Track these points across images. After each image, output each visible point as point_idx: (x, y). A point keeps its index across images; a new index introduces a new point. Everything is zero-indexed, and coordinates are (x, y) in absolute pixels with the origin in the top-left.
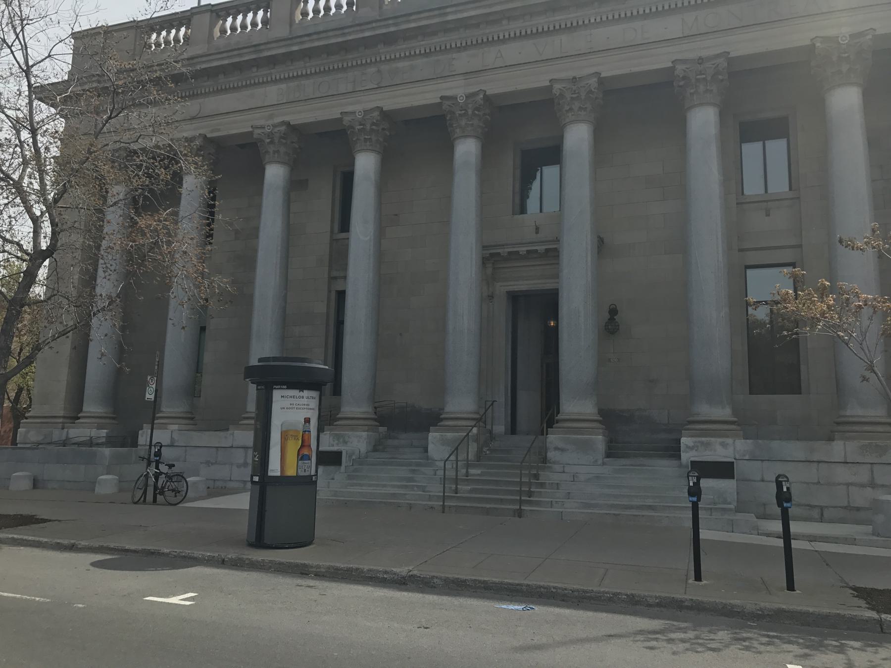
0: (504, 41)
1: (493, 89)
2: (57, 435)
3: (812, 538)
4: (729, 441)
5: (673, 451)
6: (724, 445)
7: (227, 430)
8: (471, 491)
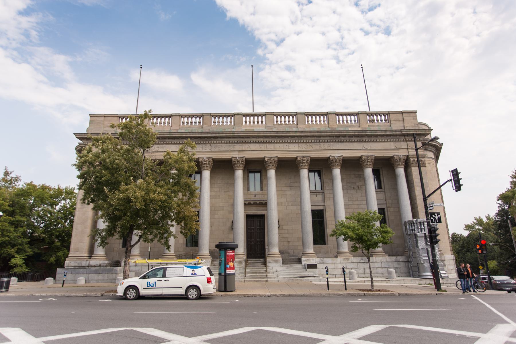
2: (84, 263)
3: (340, 282)
4: (314, 258)
5: (299, 261)
6: (313, 260)
8: (251, 276)
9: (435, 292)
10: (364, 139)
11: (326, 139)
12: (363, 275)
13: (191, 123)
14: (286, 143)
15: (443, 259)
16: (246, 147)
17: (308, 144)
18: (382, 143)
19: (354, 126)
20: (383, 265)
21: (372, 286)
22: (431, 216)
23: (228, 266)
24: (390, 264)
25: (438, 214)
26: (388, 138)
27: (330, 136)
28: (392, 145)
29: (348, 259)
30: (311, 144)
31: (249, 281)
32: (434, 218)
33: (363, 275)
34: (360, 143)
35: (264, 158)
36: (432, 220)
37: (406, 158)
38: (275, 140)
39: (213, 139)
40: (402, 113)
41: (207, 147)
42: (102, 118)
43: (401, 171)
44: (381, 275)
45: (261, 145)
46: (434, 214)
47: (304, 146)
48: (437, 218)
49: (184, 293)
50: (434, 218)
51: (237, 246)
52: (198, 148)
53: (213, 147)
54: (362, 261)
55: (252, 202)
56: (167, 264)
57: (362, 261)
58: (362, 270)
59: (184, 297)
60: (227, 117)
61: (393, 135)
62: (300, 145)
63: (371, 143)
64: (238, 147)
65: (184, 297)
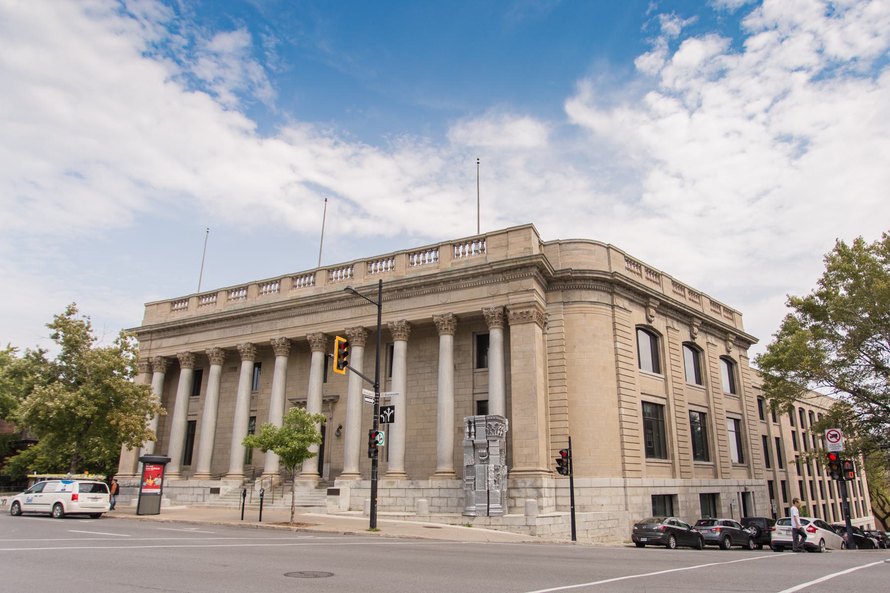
0: (294, 316)
1: (457, 312)
9: (570, 540)
10: (439, 288)
12: (411, 509)
14: (335, 309)
15: (538, 484)
16: (289, 323)
17: (363, 308)
19: (430, 269)
20: (442, 493)
22: (382, 413)
23: (145, 484)
24: (452, 491)
25: (392, 408)
26: (476, 280)
28: (484, 291)
29: (393, 483)
32: (385, 415)
33: (411, 509)
35: (482, 312)
36: (381, 419)
37: (501, 310)
38: (321, 308)
39: (252, 318)
40: (507, 232)
41: (248, 329)
42: (155, 307)
44: (437, 509)
45: (306, 317)
48: (389, 415)
51: (169, 460)
54: (411, 487)
57: (411, 487)
58: (411, 500)
59: (51, 515)
61: (483, 274)
62: (353, 310)
64: (281, 324)
65: (51, 515)
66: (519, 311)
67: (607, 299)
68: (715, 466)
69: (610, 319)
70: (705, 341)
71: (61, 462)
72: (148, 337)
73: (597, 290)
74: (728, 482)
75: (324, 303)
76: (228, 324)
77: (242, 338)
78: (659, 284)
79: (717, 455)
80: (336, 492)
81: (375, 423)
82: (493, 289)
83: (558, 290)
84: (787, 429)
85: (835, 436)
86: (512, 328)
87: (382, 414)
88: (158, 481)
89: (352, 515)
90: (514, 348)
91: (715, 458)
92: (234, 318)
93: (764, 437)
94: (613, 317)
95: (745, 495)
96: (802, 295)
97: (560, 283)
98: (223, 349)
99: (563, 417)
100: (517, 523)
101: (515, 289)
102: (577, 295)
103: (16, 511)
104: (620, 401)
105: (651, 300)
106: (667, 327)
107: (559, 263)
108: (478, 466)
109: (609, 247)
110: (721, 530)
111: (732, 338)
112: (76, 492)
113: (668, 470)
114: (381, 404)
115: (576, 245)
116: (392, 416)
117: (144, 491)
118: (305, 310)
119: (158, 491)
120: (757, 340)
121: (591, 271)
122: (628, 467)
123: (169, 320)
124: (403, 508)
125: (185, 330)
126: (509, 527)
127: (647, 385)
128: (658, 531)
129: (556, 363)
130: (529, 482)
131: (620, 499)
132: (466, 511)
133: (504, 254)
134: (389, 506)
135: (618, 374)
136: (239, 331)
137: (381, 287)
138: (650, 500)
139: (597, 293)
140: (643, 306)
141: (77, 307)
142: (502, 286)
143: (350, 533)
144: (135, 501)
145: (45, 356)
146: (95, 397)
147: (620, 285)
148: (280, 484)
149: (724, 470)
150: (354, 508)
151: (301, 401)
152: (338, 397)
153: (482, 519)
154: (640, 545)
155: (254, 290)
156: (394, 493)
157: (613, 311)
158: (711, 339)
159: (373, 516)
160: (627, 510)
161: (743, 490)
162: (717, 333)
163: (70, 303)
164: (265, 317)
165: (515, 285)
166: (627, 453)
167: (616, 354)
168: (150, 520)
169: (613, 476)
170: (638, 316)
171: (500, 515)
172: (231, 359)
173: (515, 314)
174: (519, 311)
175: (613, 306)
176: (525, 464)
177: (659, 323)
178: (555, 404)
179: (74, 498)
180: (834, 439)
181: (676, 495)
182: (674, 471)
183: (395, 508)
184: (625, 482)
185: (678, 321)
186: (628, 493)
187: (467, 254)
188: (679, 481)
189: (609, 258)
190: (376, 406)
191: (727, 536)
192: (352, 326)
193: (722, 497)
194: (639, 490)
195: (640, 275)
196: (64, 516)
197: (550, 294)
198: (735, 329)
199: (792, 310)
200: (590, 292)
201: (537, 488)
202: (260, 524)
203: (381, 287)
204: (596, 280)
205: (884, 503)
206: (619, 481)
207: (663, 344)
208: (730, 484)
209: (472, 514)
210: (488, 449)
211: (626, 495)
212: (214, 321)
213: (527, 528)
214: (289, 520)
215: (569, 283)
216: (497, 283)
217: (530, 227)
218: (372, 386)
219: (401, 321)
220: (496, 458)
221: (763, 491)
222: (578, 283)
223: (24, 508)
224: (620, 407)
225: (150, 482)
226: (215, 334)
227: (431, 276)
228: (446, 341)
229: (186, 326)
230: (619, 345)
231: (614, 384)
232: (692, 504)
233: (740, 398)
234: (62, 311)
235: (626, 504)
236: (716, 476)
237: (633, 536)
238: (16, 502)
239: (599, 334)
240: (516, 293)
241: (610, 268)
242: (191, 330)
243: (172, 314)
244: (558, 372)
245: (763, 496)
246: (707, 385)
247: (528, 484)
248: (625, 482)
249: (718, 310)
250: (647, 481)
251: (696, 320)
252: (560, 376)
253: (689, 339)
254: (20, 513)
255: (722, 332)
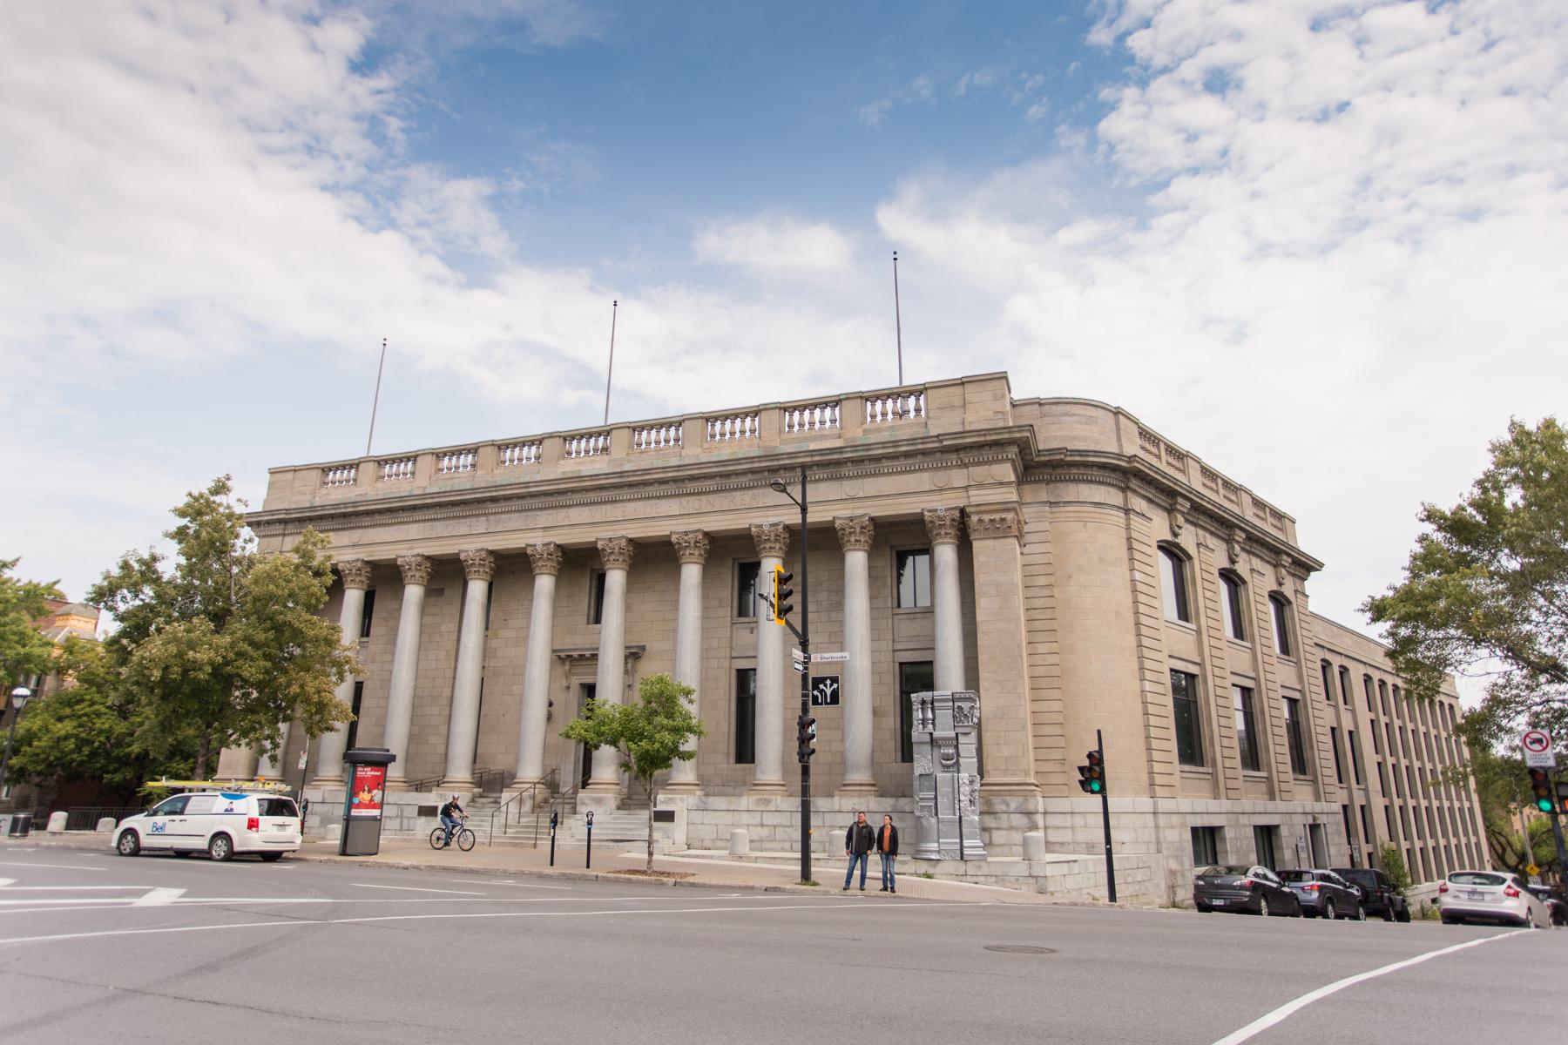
1: (876, 513)
7: (831, 795)
9: (1107, 901)
10: (845, 471)
11: (745, 480)
13: (812, 424)
15: (1031, 807)
16: (561, 517)
17: (703, 498)
18: (897, 478)
21: (650, 862)
22: (815, 687)
23: (356, 800)
26: (910, 461)
27: (753, 471)
28: (924, 480)
29: (768, 801)
30: (711, 497)
31: (500, 844)
32: (821, 691)
34: (837, 484)
37: (957, 514)
38: (625, 494)
39: (489, 505)
40: (962, 383)
41: (480, 525)
42: (290, 475)
43: (946, 554)
45: (594, 508)
46: (823, 680)
47: (693, 504)
48: (828, 691)
49: (206, 847)
50: (821, 691)
52: (335, 538)
53: (493, 523)
55: (575, 654)
56: (190, 790)
59: (204, 855)
60: (823, 409)
61: (924, 453)
62: (684, 500)
63: (867, 480)
64: (544, 519)
65: (204, 855)
66: (986, 517)
67: (1115, 497)
68: (1269, 779)
69: (1123, 533)
70: (1248, 567)
71: (72, 752)
72: (279, 529)
73: (1100, 483)
74: (1290, 807)
75: (631, 485)
76: (441, 513)
77: (470, 539)
78: (1183, 472)
79: (1218, 756)
80: (668, 816)
81: (805, 704)
82: (941, 478)
83: (1040, 481)
84: (1365, 717)
85: (1539, 741)
86: (976, 545)
87: (819, 690)
88: (377, 794)
89: (711, 857)
90: (981, 578)
91: (1269, 765)
92: (453, 504)
93: (1333, 729)
94: (1128, 528)
95: (1314, 828)
96: (1447, 506)
97: (1041, 467)
98: (428, 558)
99: (1056, 694)
100: (1014, 871)
101: (979, 480)
102: (1072, 491)
103: (129, 844)
104: (1142, 668)
105: (1180, 500)
106: (1198, 545)
107: (1052, 437)
108: (942, 776)
109: (1117, 412)
110: (1320, 889)
111: (1286, 560)
112: (255, 813)
113: (1206, 785)
114: (812, 674)
115: (1068, 407)
116: (835, 694)
117: (354, 812)
118: (593, 496)
119: (376, 812)
120: (1322, 565)
121: (1097, 453)
122: (1158, 780)
123: (318, 502)
124: (787, 846)
125: (355, 521)
126: (1000, 879)
127: (1174, 643)
128: (1242, 887)
129: (1039, 603)
130: (1014, 803)
131: (1149, 835)
132: (918, 851)
133: (959, 420)
134: (762, 841)
135: (1138, 624)
136: (462, 527)
137: (805, 478)
138: (1188, 836)
139: (1103, 488)
140: (1165, 509)
141: (229, 483)
142: (955, 473)
143: (776, 890)
144: (336, 830)
145: (159, 566)
146: (265, 644)
147: (1145, 476)
148: (546, 801)
149: (1231, 784)
150: (695, 844)
151: (588, 654)
152: (643, 648)
153: (949, 866)
154: (1204, 907)
155: (487, 455)
156: (770, 819)
157: (1128, 519)
158: (1257, 563)
159: (806, 861)
160: (1159, 851)
161: (1311, 821)
162: (1264, 553)
163: (222, 475)
164: (515, 505)
165: (979, 472)
166: (1156, 755)
167: (1134, 591)
168: (361, 864)
169: (1136, 794)
170: (1157, 526)
171: (983, 858)
172: (446, 574)
173: (980, 521)
174: (986, 517)
175: (1127, 511)
176: (1005, 772)
177: (1188, 538)
178: (1040, 671)
179: (253, 824)
180: (1537, 747)
181: (1221, 828)
182: (1216, 786)
183: (772, 845)
184: (1155, 804)
185: (1212, 533)
186: (1161, 824)
187: (828, 424)
188: (1225, 805)
189: (1118, 429)
190: (805, 677)
191: (1330, 900)
192: (684, 528)
193: (1284, 831)
194: (1175, 819)
195: (1159, 457)
196: (232, 856)
197: (1027, 488)
198: (1292, 548)
199: (1429, 528)
200: (1092, 486)
201: (1029, 814)
202: (549, 870)
203: (805, 478)
204: (1103, 467)
205: (1504, 849)
206: (1145, 803)
207: (1193, 572)
208: (1294, 806)
209: (934, 857)
210: (956, 747)
211: (1157, 827)
212: (414, 508)
213: (1032, 881)
214: (644, 868)
215: (1059, 471)
216: (948, 468)
217: (1003, 377)
218: (797, 640)
219: (776, 525)
220: (969, 761)
221: (1337, 824)
222: (1075, 471)
223: (145, 841)
224: (1142, 679)
225: (364, 796)
226: (413, 531)
227: (832, 450)
228: (691, 573)
229: (356, 514)
230: (1138, 576)
231: (1131, 640)
232: (1245, 843)
233: (1298, 664)
234: (202, 486)
235: (1158, 842)
236: (1272, 797)
237: (1195, 897)
238: (131, 831)
239: (1103, 558)
240: (980, 486)
241: (1121, 446)
242: (367, 521)
243: (324, 491)
244: (1045, 619)
245: (1339, 834)
246: (1253, 641)
247: (1013, 806)
248: (1155, 804)
249: (1155, 450)
250: (1184, 804)
251: (1238, 532)
252: (1048, 625)
253: (1226, 565)
254: (137, 852)
255: (1261, 545)
